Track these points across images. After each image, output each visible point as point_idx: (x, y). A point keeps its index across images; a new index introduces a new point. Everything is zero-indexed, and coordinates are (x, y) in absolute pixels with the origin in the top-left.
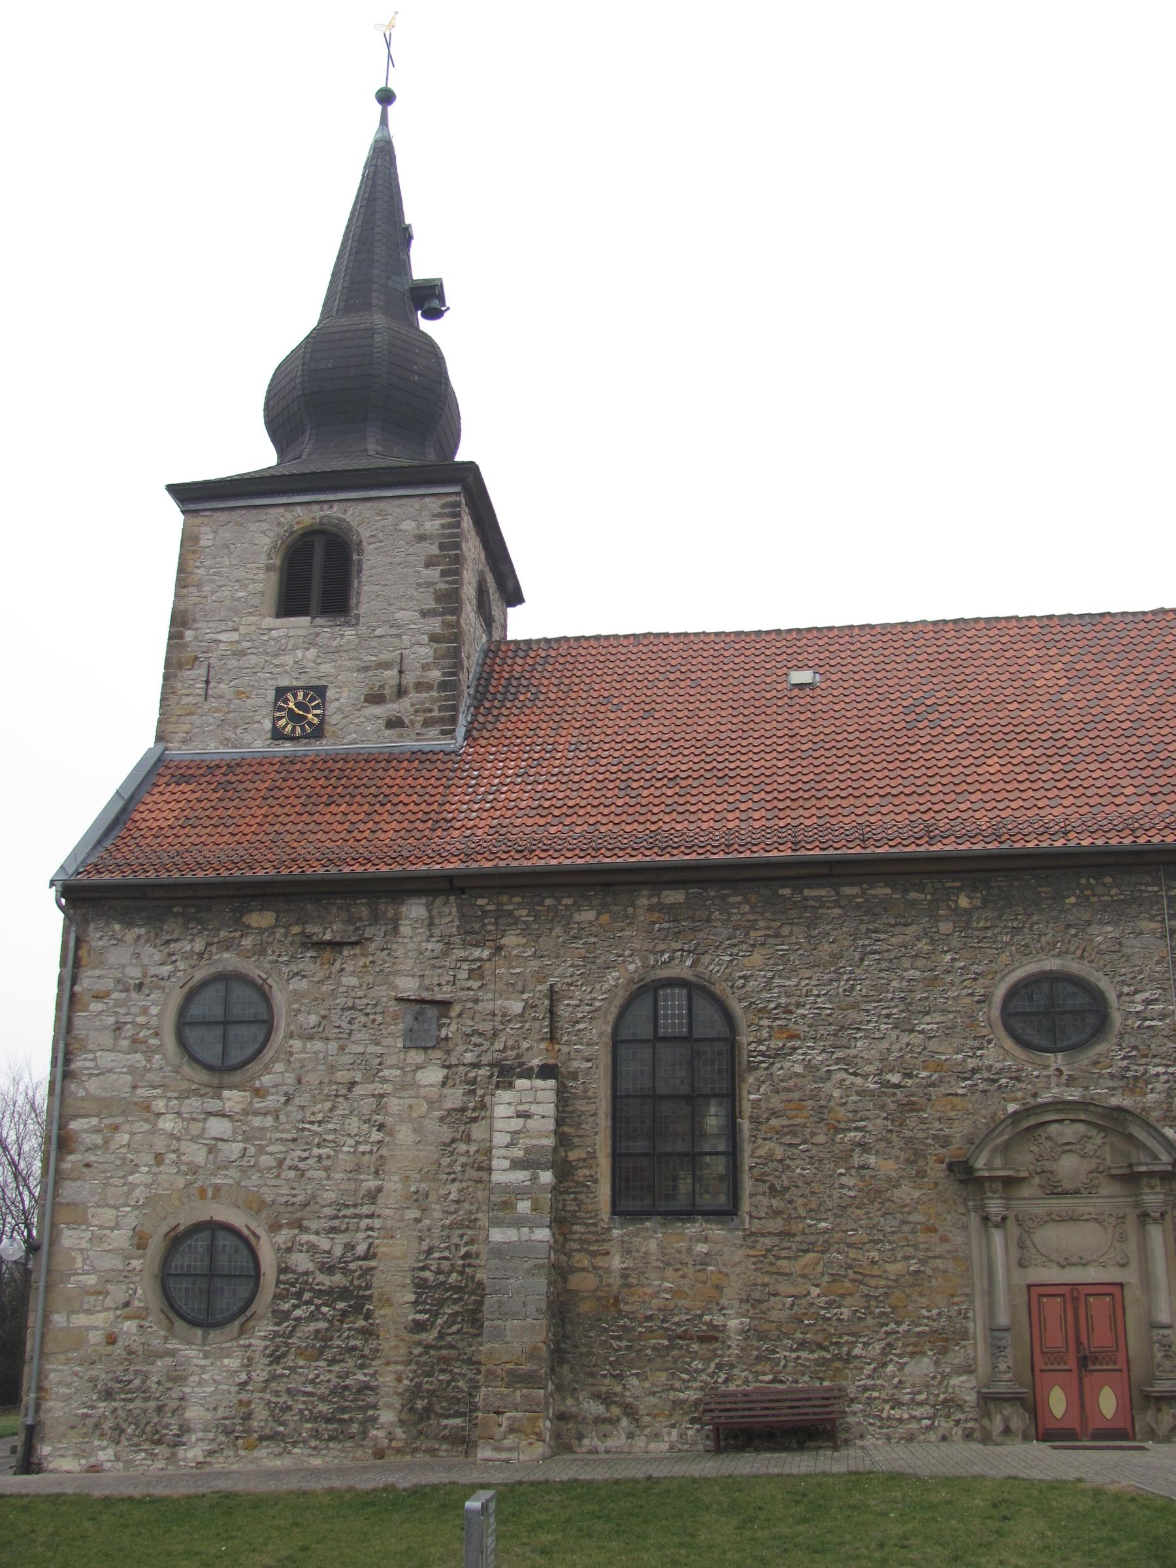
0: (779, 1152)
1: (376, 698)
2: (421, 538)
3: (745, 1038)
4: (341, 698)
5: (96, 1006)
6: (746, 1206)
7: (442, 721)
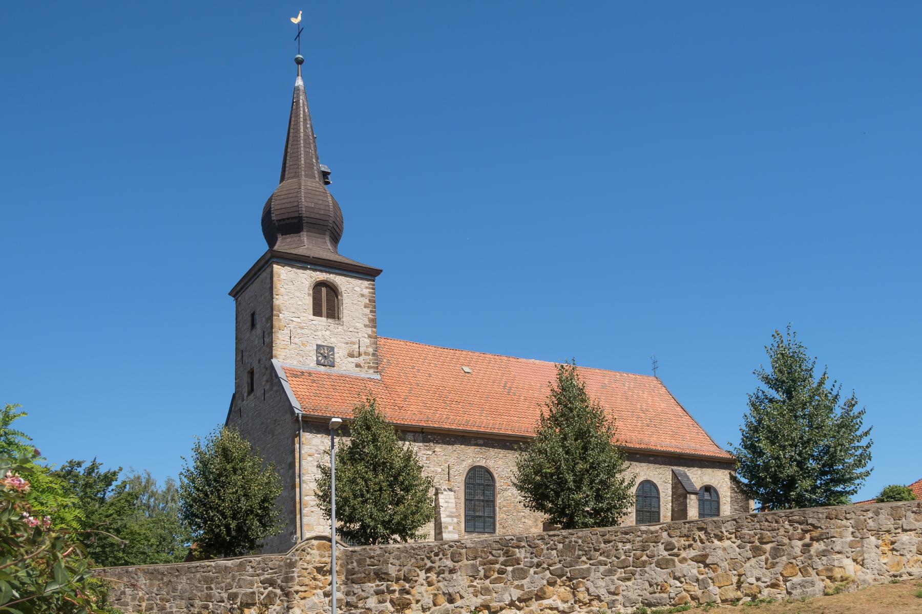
0: (505, 517)
1: (351, 355)
2: (362, 295)
3: (497, 484)
4: (340, 354)
5: (310, 458)
6: (497, 531)
7: (373, 367)
